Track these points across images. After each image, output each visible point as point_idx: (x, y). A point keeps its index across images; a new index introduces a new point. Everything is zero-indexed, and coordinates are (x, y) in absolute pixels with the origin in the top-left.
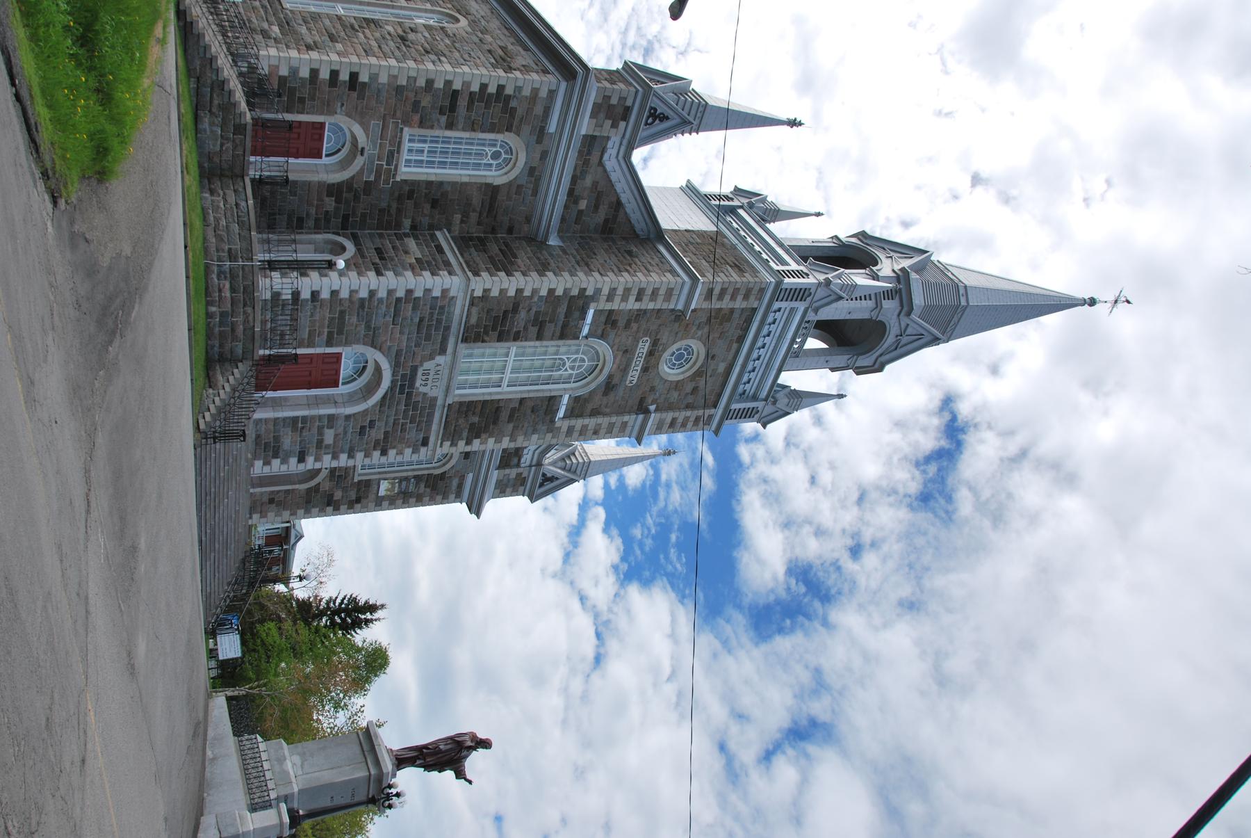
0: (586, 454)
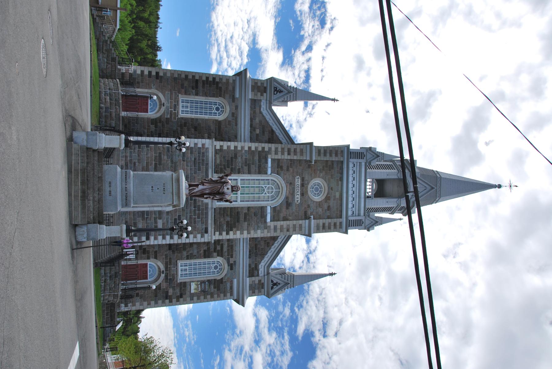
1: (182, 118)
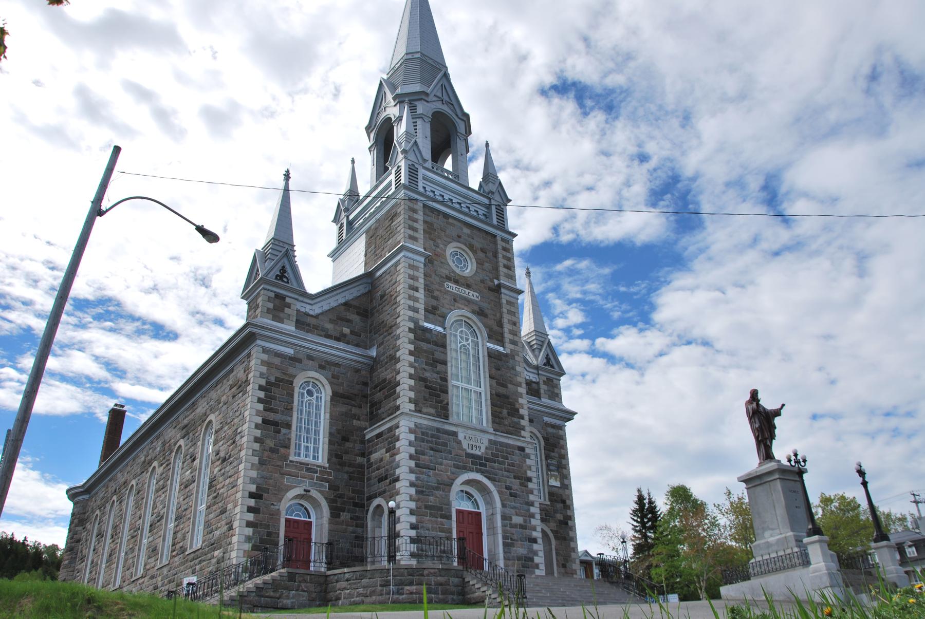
0: (529, 333)
1: (328, 460)
